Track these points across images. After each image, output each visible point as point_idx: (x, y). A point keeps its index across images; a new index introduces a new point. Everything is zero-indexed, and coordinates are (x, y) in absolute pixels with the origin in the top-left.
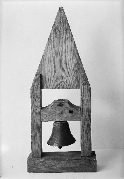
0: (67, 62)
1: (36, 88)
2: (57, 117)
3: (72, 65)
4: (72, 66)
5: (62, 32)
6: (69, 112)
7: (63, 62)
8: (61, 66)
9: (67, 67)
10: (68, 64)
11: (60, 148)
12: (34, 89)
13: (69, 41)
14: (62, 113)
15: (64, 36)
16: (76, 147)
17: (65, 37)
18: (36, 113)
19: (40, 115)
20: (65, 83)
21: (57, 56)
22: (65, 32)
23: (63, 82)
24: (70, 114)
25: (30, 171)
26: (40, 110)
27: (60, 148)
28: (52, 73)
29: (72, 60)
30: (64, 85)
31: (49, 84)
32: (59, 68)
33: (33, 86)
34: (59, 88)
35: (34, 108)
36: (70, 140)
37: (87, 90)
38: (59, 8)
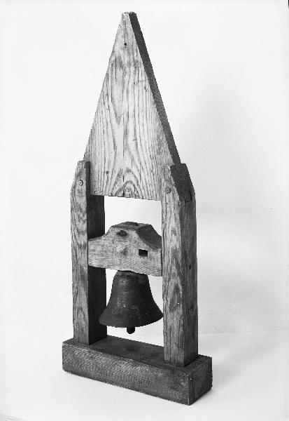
0: (138, 137)
1: (79, 191)
2: (117, 260)
3: (147, 145)
4: (148, 147)
5: (127, 69)
6: (138, 252)
7: (131, 137)
8: (126, 147)
9: (137, 148)
10: (138, 141)
11: (131, 331)
12: (77, 193)
13: (140, 88)
14: (125, 253)
15: (132, 78)
16: (151, 335)
17: (133, 82)
18: (80, 247)
19: (86, 252)
20: (134, 185)
21: (119, 123)
22: (132, 69)
23: (131, 182)
24: (141, 259)
25: (72, 366)
26: (86, 241)
27: (131, 331)
28: (109, 163)
29: (146, 134)
30: (133, 189)
31: (105, 185)
32: (103, 238)
33: (74, 187)
34: (124, 195)
35: (76, 234)
36: (149, 314)
37: (172, 206)
38: (121, 17)
